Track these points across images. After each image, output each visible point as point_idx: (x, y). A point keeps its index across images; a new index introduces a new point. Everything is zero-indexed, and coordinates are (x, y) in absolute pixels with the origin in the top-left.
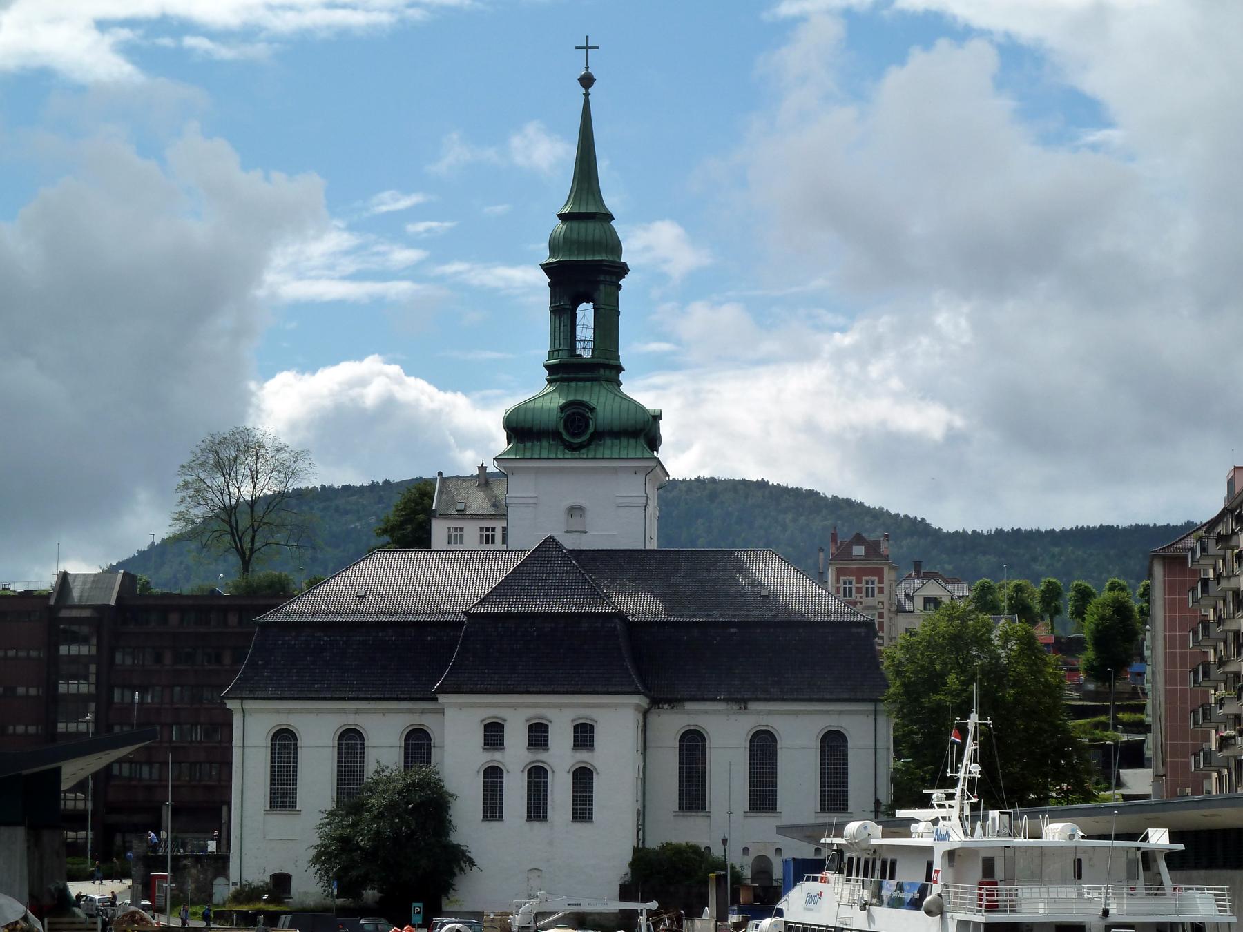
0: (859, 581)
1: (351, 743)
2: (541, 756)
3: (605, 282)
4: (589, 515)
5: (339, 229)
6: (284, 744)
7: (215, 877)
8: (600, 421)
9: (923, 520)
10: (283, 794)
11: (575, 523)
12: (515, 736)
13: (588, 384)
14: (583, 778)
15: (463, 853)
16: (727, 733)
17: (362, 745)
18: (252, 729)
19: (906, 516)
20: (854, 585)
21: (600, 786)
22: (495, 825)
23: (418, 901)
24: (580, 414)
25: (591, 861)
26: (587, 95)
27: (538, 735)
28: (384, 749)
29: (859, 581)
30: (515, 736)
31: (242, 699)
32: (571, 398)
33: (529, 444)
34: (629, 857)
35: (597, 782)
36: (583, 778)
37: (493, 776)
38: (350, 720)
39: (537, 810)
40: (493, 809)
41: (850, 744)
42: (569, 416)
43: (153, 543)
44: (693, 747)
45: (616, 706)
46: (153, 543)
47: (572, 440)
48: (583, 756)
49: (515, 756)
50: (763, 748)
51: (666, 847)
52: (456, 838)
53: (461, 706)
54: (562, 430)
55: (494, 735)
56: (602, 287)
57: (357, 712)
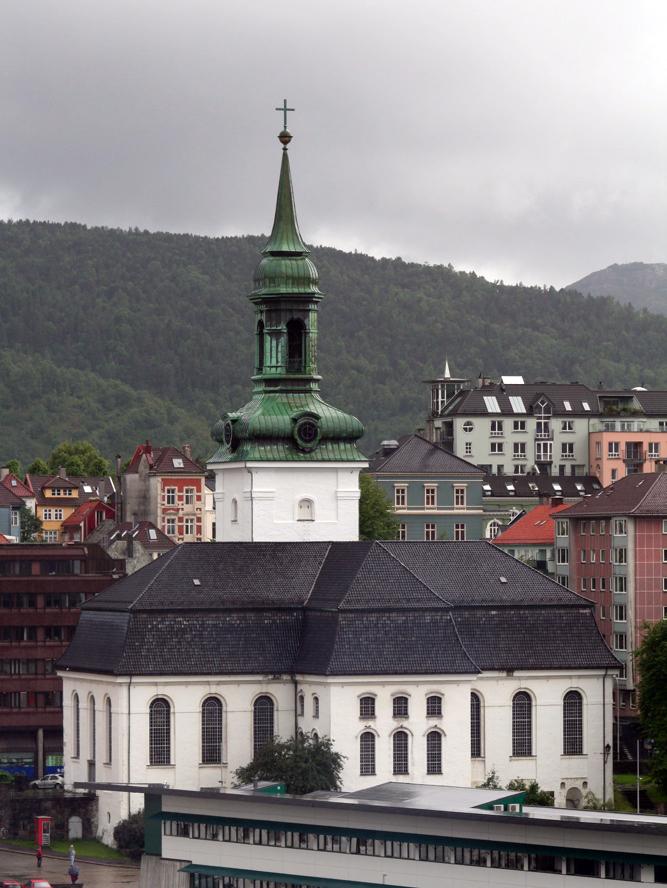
0: (180, 490)
2: (405, 724)
7: (70, 816)
8: (325, 426)
14: (435, 738)
17: (221, 710)
20: (177, 494)
21: (446, 745)
24: (310, 424)
26: (285, 149)
27: (401, 706)
29: (180, 490)
37: (368, 739)
41: (585, 701)
45: (457, 682)
48: (434, 722)
49: (384, 724)
53: (343, 684)
55: (367, 707)
57: (219, 683)
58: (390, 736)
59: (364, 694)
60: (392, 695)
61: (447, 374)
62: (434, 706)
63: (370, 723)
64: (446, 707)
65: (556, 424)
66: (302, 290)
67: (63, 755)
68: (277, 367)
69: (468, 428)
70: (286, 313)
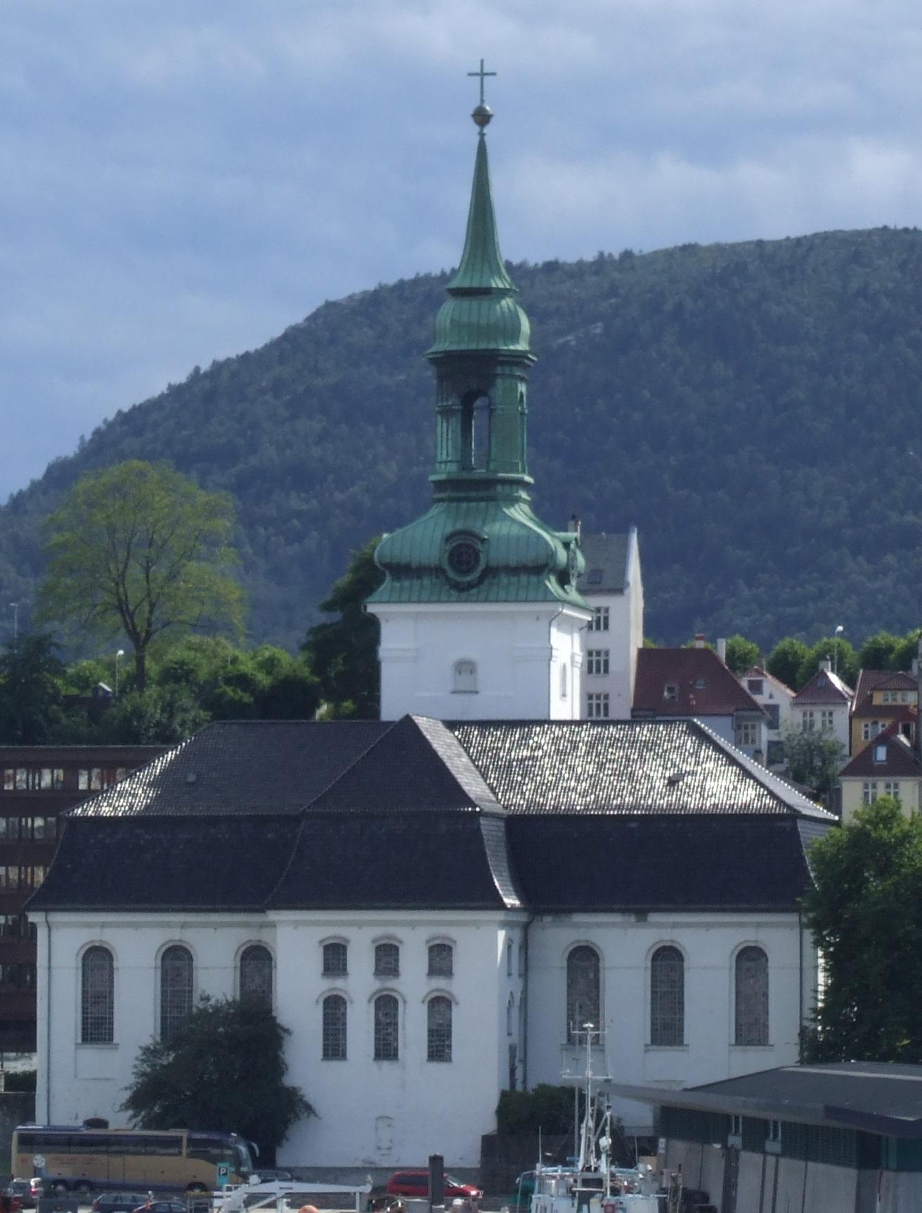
2: (392, 983)
3: (503, 376)
4: (481, 672)
6: (97, 962)
12: (361, 962)
13: (483, 504)
14: (440, 1005)
15: (301, 1100)
16: (625, 945)
18: (61, 941)
22: (335, 1065)
24: (468, 546)
25: (448, 1108)
26: (482, 135)
27: (387, 957)
30: (361, 962)
31: (47, 910)
32: (459, 526)
33: (407, 583)
34: (493, 1102)
36: (440, 1005)
37: (334, 1008)
38: (175, 935)
39: (386, 1049)
40: (334, 1047)
42: (454, 549)
43: (197, 369)
44: (584, 961)
46: (197, 369)
47: (458, 579)
48: (440, 983)
49: (360, 982)
50: (667, 962)
51: (543, 1089)
53: (297, 924)
54: (446, 567)
55: (335, 958)
56: (499, 381)
57: (759, 925)
58: (369, 1001)
59: (335, 937)
60: (373, 942)
63: (339, 983)
64: (461, 961)
66: (483, 346)
68: (446, 462)
70: (470, 376)
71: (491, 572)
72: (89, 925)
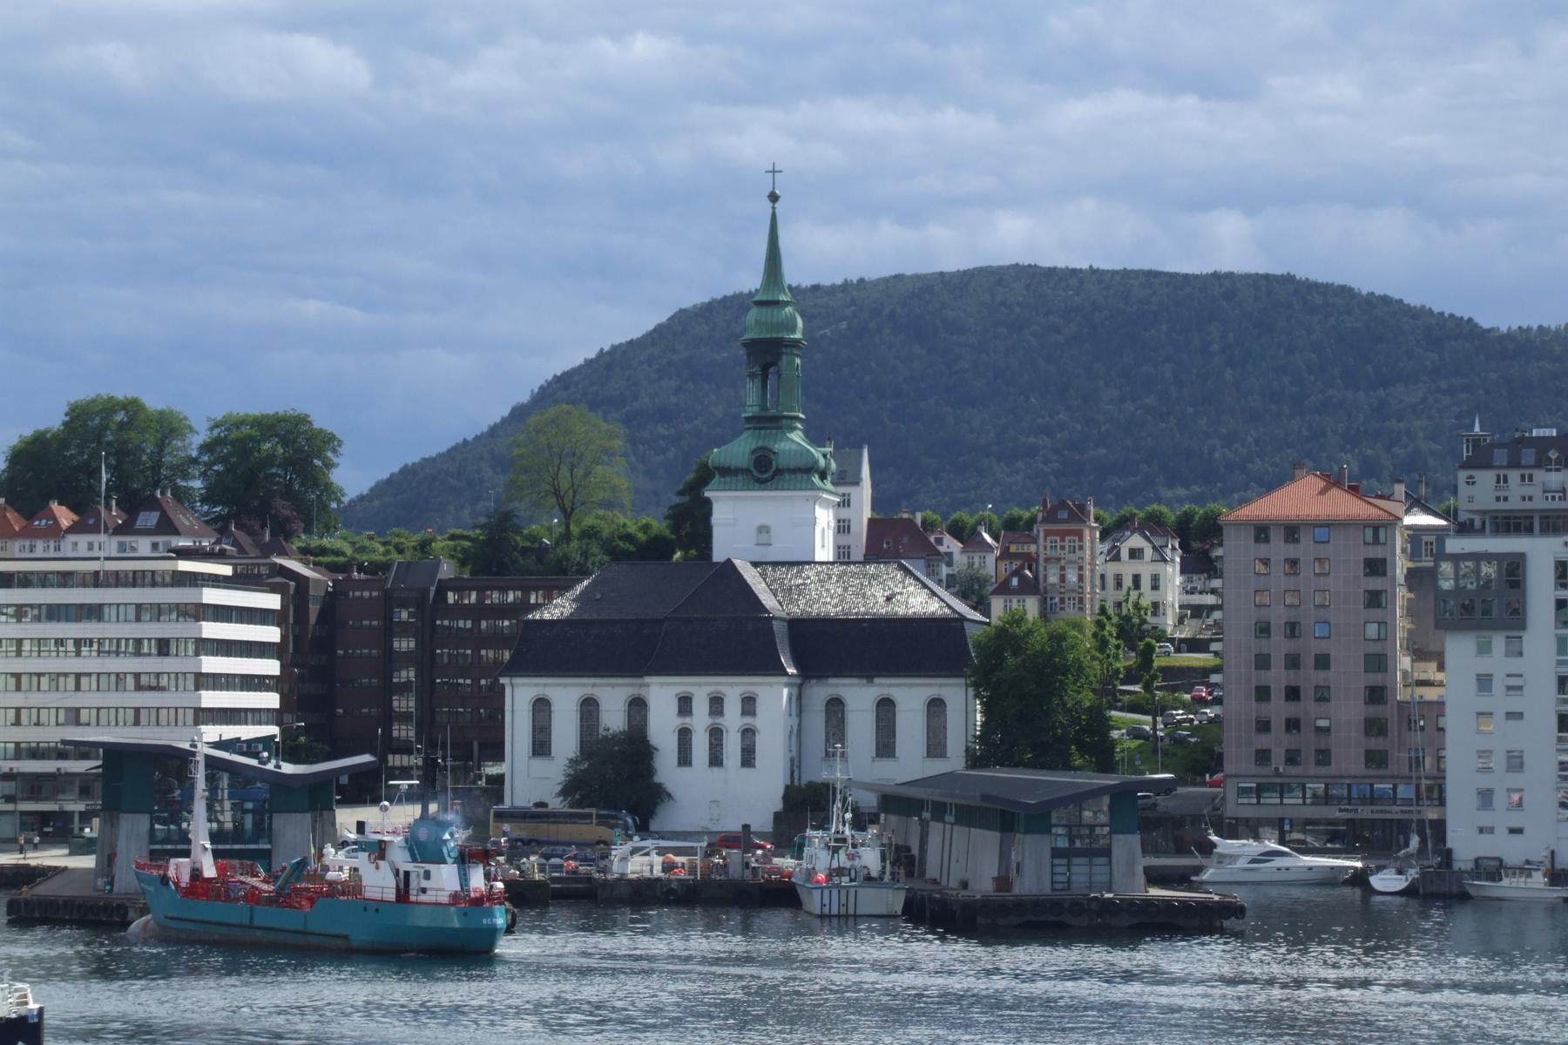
0: (1062, 540)
1: (589, 708)
5: (216, 970)
6: (542, 707)
9: (1470, 320)
10: (541, 747)
11: (764, 538)
12: (701, 707)
14: (748, 733)
16: (860, 697)
18: (520, 695)
19: (1452, 316)
21: (761, 742)
22: (685, 769)
23: (210, 880)
27: (716, 704)
28: (613, 718)
29: (1062, 540)
30: (701, 707)
32: (760, 444)
35: (759, 739)
36: (748, 733)
37: (684, 735)
38: (588, 691)
39: (716, 760)
40: (685, 759)
44: (835, 707)
48: (748, 720)
49: (700, 720)
50: (886, 707)
52: (658, 779)
53: (662, 684)
55: (685, 705)
61: (1477, 428)
62: (749, 705)
63: (688, 720)
65: (1514, 475)
67: (787, 787)
69: (1471, 482)
70: (767, 354)
71: (779, 472)
72: (536, 685)
